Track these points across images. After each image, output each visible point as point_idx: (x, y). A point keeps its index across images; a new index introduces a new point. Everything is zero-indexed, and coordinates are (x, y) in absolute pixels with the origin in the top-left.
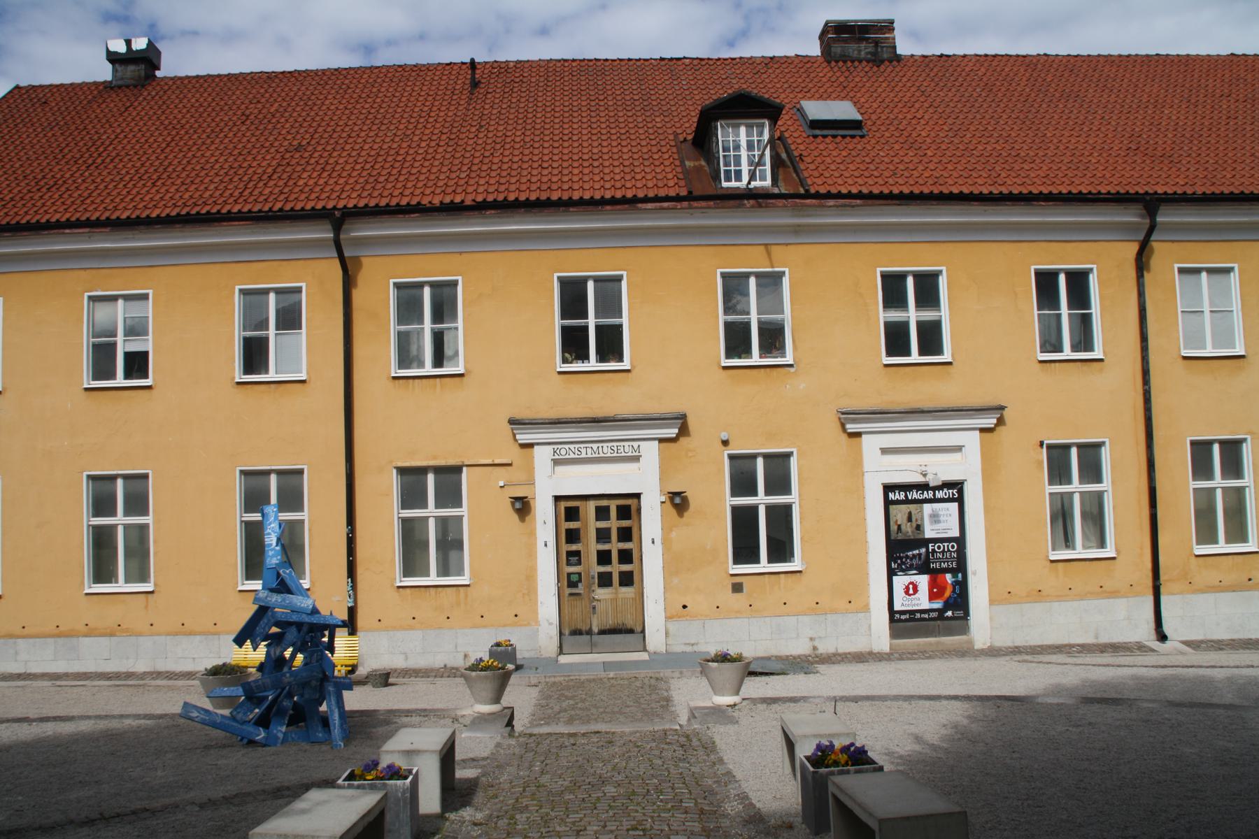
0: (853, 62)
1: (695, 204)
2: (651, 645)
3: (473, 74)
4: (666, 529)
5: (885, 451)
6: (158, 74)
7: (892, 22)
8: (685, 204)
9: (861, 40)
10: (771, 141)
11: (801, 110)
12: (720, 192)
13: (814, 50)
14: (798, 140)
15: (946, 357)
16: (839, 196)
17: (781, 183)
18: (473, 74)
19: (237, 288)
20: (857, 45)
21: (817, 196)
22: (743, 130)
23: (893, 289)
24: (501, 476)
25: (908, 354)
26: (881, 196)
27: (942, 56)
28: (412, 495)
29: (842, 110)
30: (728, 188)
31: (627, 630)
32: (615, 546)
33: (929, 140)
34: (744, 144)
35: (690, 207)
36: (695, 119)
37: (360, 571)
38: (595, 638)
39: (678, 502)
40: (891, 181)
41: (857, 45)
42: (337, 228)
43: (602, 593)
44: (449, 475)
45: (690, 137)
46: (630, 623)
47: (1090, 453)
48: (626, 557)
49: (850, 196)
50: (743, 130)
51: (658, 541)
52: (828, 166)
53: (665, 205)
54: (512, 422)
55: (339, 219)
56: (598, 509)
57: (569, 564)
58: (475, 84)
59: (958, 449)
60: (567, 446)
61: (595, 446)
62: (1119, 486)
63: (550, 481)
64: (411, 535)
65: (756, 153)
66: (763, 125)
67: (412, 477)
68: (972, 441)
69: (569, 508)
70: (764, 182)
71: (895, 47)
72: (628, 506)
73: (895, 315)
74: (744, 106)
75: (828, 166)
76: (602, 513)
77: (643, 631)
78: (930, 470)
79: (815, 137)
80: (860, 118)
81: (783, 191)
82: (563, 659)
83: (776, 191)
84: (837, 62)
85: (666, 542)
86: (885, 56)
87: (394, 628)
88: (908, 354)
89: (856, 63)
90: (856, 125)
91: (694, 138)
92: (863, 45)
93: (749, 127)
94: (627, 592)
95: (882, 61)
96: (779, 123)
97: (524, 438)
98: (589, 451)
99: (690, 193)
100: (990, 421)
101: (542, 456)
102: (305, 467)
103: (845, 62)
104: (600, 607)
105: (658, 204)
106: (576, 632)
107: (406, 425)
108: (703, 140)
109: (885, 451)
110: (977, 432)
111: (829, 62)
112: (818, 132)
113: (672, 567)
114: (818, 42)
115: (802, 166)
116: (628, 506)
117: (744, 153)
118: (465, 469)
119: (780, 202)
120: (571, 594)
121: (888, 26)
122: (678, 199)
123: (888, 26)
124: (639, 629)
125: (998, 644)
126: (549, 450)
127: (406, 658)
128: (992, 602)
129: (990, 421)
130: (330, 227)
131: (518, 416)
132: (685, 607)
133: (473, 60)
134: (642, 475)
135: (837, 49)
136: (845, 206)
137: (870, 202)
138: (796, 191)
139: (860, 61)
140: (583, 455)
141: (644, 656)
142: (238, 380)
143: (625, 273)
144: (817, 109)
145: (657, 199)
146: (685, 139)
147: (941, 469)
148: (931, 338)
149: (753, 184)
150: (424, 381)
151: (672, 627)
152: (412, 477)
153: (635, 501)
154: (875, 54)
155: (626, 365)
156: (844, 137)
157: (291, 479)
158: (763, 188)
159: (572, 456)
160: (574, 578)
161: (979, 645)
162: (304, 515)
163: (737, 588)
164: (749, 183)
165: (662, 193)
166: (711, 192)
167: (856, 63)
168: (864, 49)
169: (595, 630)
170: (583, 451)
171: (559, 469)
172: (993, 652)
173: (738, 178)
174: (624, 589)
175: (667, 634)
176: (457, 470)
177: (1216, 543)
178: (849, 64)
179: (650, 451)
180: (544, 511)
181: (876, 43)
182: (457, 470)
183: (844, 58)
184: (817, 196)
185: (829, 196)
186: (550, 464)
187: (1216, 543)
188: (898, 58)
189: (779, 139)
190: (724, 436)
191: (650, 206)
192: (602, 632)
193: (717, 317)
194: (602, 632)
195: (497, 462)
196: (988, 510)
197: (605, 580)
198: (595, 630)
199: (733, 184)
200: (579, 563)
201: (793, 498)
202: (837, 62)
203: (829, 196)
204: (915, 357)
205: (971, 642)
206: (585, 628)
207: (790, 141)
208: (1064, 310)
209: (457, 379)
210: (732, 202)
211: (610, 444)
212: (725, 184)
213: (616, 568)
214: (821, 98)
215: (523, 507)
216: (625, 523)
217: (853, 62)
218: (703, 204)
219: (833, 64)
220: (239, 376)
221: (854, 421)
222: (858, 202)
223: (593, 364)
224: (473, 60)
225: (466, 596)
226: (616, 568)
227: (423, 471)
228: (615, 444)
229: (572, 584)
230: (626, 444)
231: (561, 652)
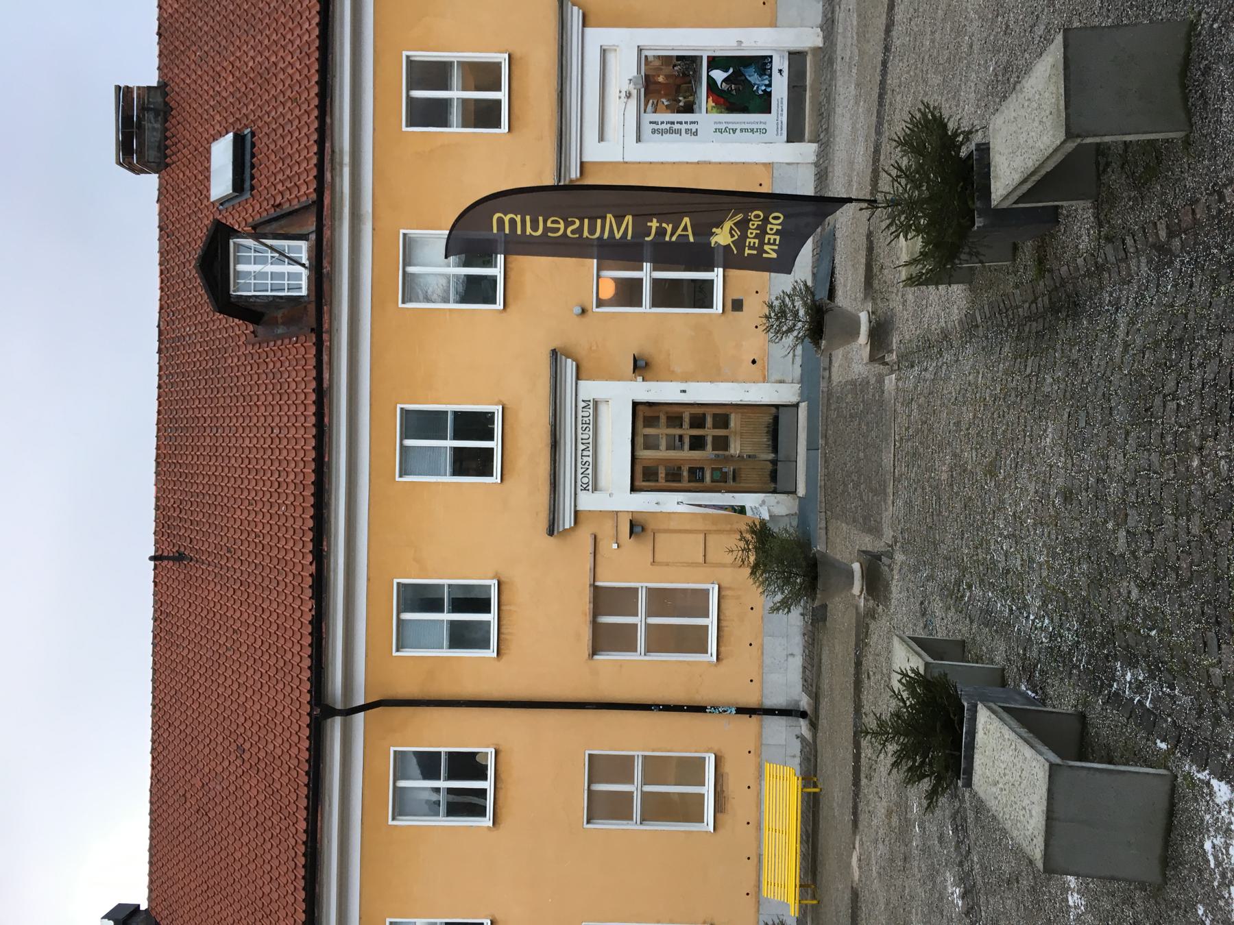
0: (166, 138)
1: (326, 326)
2: (794, 399)
3: (168, 558)
4: (671, 377)
5: (602, 138)
6: (144, 906)
7: (118, 88)
8: (325, 337)
9: (140, 126)
10: (257, 237)
11: (224, 201)
12: (313, 298)
13: (151, 182)
14: (256, 209)
15: (503, 58)
16: (320, 166)
17: (304, 231)
18: (168, 558)
19: (391, 822)
20: (147, 130)
21: (320, 191)
22: (240, 267)
23: (430, 114)
24: (609, 547)
25: (498, 102)
26: (322, 118)
27: (159, 34)
28: (622, 639)
29: (222, 152)
30: (309, 289)
31: (774, 419)
32: (688, 432)
33: (259, 59)
34: (258, 268)
35: (330, 332)
36: (236, 320)
37: (699, 699)
38: (781, 455)
39: (641, 367)
40: (305, 106)
41: (147, 130)
42: (331, 712)
43: (735, 448)
44: (604, 600)
45: (251, 327)
46: (768, 419)
47: (599, 767)
48: (698, 422)
49: (321, 153)
50: (240, 267)
51: (683, 386)
52: (288, 182)
53: (325, 358)
54: (551, 532)
55: (322, 711)
56: (647, 447)
57: (702, 480)
58: (179, 557)
59: (604, 52)
60: (580, 476)
61: (581, 447)
62: (637, 670)
63: (614, 493)
64: (662, 640)
65: (269, 255)
66: (237, 246)
67: (604, 639)
68: (597, 37)
69: (644, 477)
70: (302, 249)
71: (149, 88)
72: (644, 413)
73: (455, 114)
74: (214, 263)
75: (288, 182)
76: (651, 444)
77: (777, 406)
78: (626, 87)
79: (252, 188)
80: (231, 135)
81: (314, 228)
82: (801, 491)
83: (313, 237)
84: (166, 156)
85: (686, 378)
86: (160, 100)
87: (761, 666)
88: (498, 103)
89: (168, 134)
90: (239, 142)
91: (252, 322)
92: (147, 125)
93: (238, 261)
94: (734, 421)
95: (166, 104)
96: (236, 227)
97: (568, 522)
98: (585, 453)
99: (312, 330)
100: (570, 367)
101: (588, 502)
102: (587, 752)
103: (167, 147)
104: (749, 450)
105: (325, 366)
106: (774, 476)
107: (544, 642)
108: (253, 312)
109: (602, 138)
110: (588, 30)
111: (167, 165)
112: (247, 185)
113: (714, 375)
114: (143, 176)
115: (286, 206)
116: (644, 413)
117: (270, 268)
118: (598, 584)
119: (327, 233)
120: (734, 480)
121: (124, 94)
122: (319, 345)
123: (124, 94)
124: (774, 410)
125: (819, 19)
126: (582, 496)
127: (792, 655)
128: (773, 24)
129: (570, 367)
130: (329, 720)
131: (543, 524)
132: (754, 362)
133: (151, 558)
134: (615, 399)
135: (152, 155)
136: (332, 160)
137: (328, 132)
138: (312, 216)
139: (166, 130)
140: (590, 459)
141: (803, 406)
142: (491, 824)
143: (399, 406)
144: (221, 183)
145: (319, 367)
146: (253, 332)
147: (624, 71)
148: (485, 75)
149: (304, 261)
150: (502, 623)
151: (773, 378)
152: (604, 639)
153: (640, 408)
154: (157, 113)
155: (497, 409)
156: (253, 156)
157: (599, 767)
158: (309, 251)
159: (590, 471)
160: (717, 475)
161: (819, 42)
162: (646, 307)
163: (738, 305)
164: (303, 265)
165: (313, 362)
166: (312, 308)
167: (168, 134)
168: (152, 126)
169: (771, 456)
170: (585, 459)
171: (603, 482)
172: (829, 26)
173: (298, 276)
174: (732, 424)
175: (781, 382)
176: (597, 592)
177: (712, 281)
178: (168, 142)
179: (590, 389)
180: (645, 502)
181: (143, 108)
182: (596, 589)
183: (162, 148)
184: (320, 191)
185: (320, 178)
186: (597, 494)
187: (712, 281)
188: (163, 86)
189: (254, 228)
190: (578, 310)
191: (326, 376)
192: (775, 449)
193: (450, 310)
194: (775, 449)
195: (591, 549)
196: (672, 23)
197: (722, 443)
198: (771, 456)
199: (304, 283)
200: (702, 469)
201: (638, 754)
202: (166, 156)
203: (320, 178)
204: (502, 95)
205: (816, 50)
206: (770, 466)
207: (257, 217)
208: (447, 616)
209: (503, 587)
210: (326, 286)
211: (580, 431)
212: (304, 292)
213: (709, 432)
214: (208, 178)
215: (637, 527)
216: (720, 432)
217: (166, 138)
218: (326, 317)
219: (168, 160)
220: (487, 822)
221: (568, 170)
222: (328, 145)
223: (495, 444)
224: (151, 558)
225: (730, 588)
226: (709, 432)
227: (595, 625)
228: (580, 426)
229: (724, 478)
230: (580, 414)
231: (795, 492)
